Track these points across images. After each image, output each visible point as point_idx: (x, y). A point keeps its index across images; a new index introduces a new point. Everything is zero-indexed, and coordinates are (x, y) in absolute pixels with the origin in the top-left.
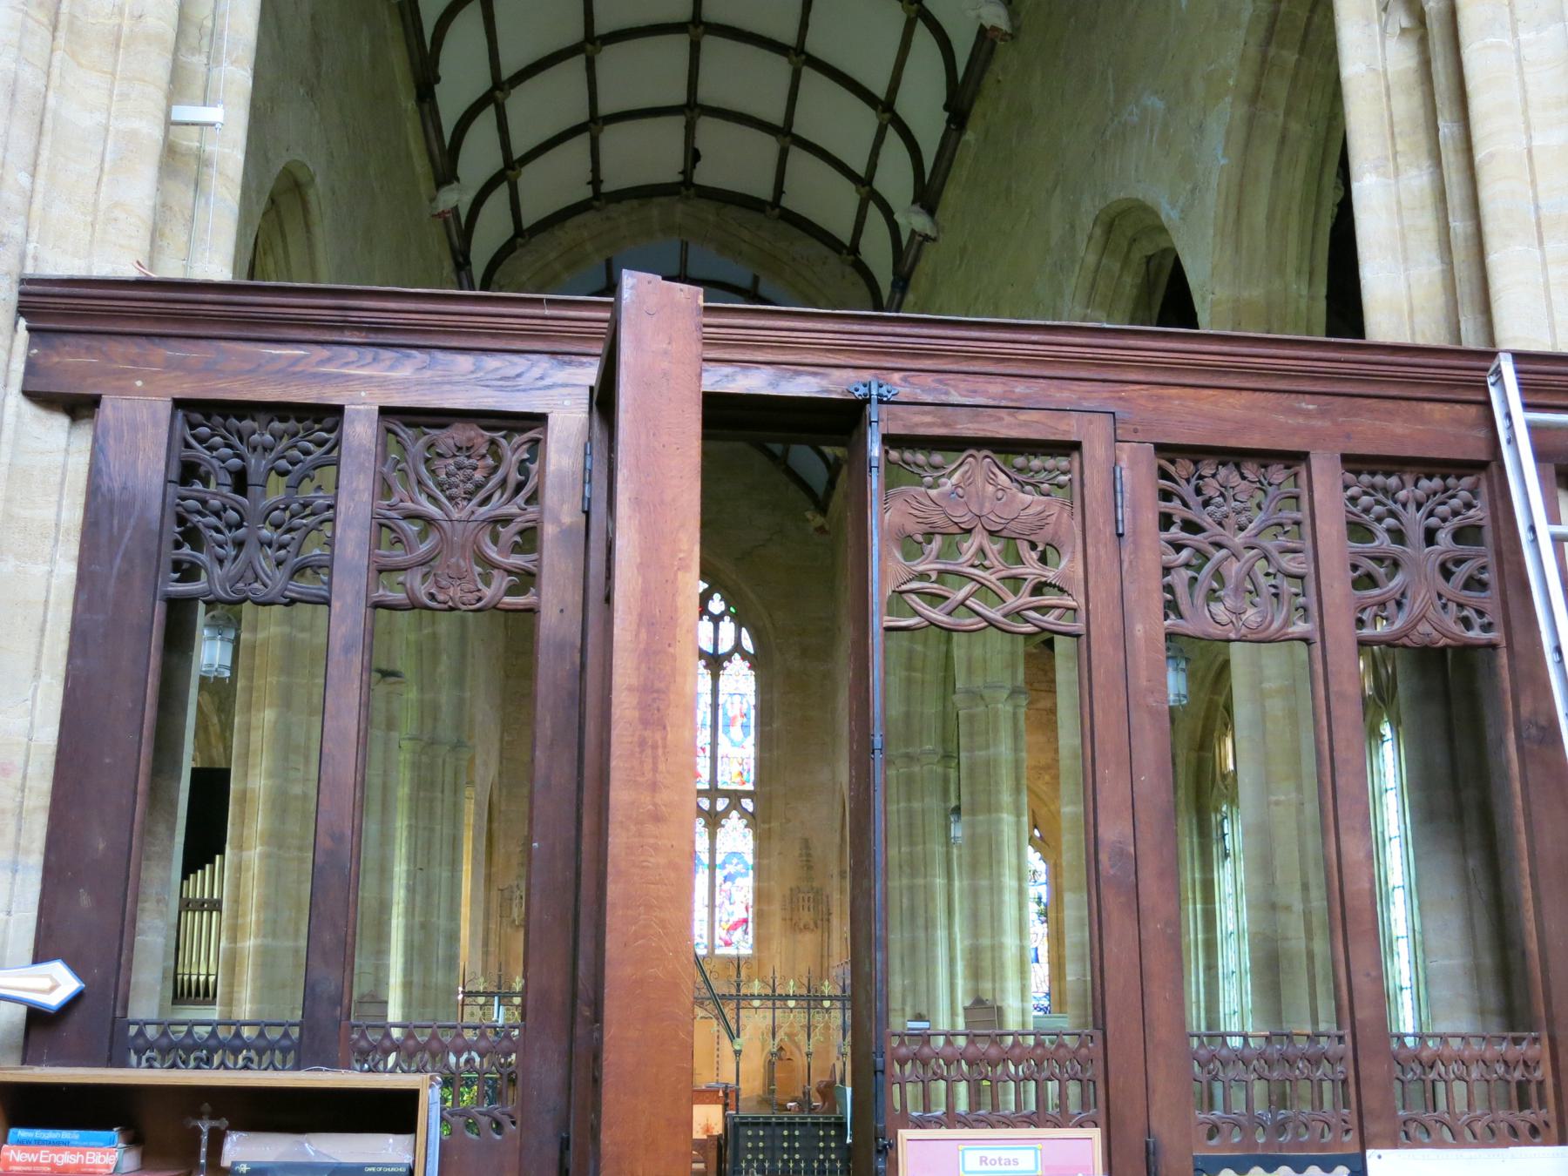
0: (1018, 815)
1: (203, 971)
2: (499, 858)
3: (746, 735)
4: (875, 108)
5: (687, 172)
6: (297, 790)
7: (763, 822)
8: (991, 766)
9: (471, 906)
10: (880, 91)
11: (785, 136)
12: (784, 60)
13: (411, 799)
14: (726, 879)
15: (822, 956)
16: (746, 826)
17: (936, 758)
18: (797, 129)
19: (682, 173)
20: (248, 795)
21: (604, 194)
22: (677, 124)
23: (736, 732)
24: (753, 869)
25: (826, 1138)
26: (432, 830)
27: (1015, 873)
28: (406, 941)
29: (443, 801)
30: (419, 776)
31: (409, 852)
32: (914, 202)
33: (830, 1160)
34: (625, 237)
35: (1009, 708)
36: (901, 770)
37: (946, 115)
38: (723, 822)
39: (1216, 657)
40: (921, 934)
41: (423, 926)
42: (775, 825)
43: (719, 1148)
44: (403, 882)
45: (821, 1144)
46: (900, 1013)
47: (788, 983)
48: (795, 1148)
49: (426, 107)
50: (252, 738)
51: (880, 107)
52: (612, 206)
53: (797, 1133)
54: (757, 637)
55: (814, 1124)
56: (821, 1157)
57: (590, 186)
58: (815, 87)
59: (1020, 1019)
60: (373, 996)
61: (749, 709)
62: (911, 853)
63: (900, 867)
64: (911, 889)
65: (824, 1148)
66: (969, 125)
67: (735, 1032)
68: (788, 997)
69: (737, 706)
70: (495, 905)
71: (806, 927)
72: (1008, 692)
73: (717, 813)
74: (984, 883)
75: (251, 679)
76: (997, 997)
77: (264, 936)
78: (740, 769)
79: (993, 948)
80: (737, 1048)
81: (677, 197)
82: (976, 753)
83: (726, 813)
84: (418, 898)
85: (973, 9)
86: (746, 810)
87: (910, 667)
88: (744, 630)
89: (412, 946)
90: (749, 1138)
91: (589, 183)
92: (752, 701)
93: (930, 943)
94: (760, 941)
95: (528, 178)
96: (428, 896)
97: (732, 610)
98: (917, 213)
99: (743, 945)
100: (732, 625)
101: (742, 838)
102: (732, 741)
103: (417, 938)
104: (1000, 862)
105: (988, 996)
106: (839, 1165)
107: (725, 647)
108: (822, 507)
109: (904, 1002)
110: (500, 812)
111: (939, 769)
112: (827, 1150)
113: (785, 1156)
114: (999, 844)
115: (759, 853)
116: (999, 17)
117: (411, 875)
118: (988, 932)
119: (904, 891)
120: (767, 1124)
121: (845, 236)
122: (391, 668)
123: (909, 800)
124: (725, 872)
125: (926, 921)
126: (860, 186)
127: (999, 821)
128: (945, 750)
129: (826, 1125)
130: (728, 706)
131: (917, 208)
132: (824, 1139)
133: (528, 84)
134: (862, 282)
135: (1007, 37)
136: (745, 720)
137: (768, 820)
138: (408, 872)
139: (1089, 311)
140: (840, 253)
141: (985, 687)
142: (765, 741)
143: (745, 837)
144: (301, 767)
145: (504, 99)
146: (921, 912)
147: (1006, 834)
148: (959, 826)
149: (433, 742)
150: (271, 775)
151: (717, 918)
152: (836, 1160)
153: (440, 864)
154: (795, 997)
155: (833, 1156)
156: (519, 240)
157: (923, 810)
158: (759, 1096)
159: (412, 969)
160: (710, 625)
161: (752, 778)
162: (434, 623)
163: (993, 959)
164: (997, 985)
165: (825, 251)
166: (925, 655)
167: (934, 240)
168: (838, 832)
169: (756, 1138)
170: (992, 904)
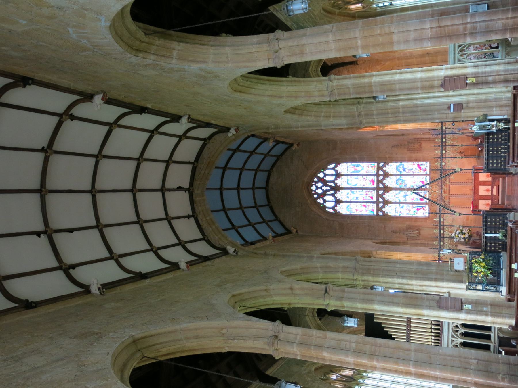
0: (373, 76)
1: (430, 337)
4: (153, 136)
5: (185, 190)
6: (354, 345)
7: (387, 159)
8: (355, 87)
10: (148, 135)
11: (169, 162)
12: (142, 164)
14: (405, 171)
15: (430, 140)
16: (388, 165)
17: (359, 106)
19: (185, 191)
20: (356, 363)
21: (193, 214)
22: (167, 194)
23: (359, 169)
24: (401, 163)
25: (493, 139)
26: (384, 270)
27: (394, 76)
30: (366, 273)
31: (390, 278)
32: (179, 123)
33: (501, 137)
34: (205, 208)
35: (336, 81)
36: (363, 118)
37: (143, 114)
38: (387, 172)
39: (322, 14)
40: (419, 109)
44: (400, 280)
45: (496, 140)
46: (448, 115)
48: (497, 149)
49: (148, 276)
51: (152, 134)
52: (196, 211)
58: (150, 153)
59: (449, 70)
60: (438, 302)
61: (352, 165)
62: (392, 114)
63: (396, 117)
65: (497, 139)
66: (144, 106)
67: (454, 171)
68: (441, 153)
69: (351, 168)
70: (413, 242)
71: (420, 146)
72: (329, 82)
73: (384, 174)
74: (397, 86)
75: (314, 358)
76: (440, 79)
77: (409, 364)
78: (370, 167)
79: (422, 82)
80: (459, 170)
81: (193, 192)
83: (384, 171)
84: (406, 275)
85: (97, 106)
86: (383, 165)
87: (329, 117)
88: (328, 167)
89: (422, 278)
90: (493, 165)
91: (189, 219)
92: (349, 164)
93: (423, 105)
94: (425, 160)
96: (405, 272)
97: (322, 170)
98: (182, 121)
99: (426, 165)
100: (327, 170)
101: (392, 166)
102: (362, 170)
103: (420, 276)
104: (390, 81)
105: (440, 82)
106: (503, 134)
108: (291, 145)
109: (443, 113)
110: (384, 239)
111: (363, 105)
113: (500, 153)
114: (383, 82)
115: (396, 161)
116: (99, 98)
120: (488, 159)
121: (201, 143)
122: (324, 290)
123: (373, 115)
124: (403, 171)
125: (415, 107)
126: (182, 139)
127: (375, 82)
128: (357, 104)
129: (488, 139)
130: (351, 171)
131: (180, 121)
134: (214, 137)
135: (105, 94)
136: (355, 166)
137: (386, 159)
138: (397, 278)
139: (174, 57)
140: (206, 144)
141: (328, 90)
142: (362, 160)
143: (391, 165)
144: (345, 343)
145: (156, 247)
146: (411, 109)
147: (379, 80)
148: (380, 97)
149: (355, 268)
150: (347, 356)
151: (417, 173)
152: (501, 135)
155: (500, 136)
158: (476, 159)
159: (430, 278)
160: (327, 177)
161: (373, 163)
163: (425, 81)
165: (206, 148)
166: (325, 112)
167: (189, 115)
168: (389, 136)
169: (493, 163)
170: (405, 83)
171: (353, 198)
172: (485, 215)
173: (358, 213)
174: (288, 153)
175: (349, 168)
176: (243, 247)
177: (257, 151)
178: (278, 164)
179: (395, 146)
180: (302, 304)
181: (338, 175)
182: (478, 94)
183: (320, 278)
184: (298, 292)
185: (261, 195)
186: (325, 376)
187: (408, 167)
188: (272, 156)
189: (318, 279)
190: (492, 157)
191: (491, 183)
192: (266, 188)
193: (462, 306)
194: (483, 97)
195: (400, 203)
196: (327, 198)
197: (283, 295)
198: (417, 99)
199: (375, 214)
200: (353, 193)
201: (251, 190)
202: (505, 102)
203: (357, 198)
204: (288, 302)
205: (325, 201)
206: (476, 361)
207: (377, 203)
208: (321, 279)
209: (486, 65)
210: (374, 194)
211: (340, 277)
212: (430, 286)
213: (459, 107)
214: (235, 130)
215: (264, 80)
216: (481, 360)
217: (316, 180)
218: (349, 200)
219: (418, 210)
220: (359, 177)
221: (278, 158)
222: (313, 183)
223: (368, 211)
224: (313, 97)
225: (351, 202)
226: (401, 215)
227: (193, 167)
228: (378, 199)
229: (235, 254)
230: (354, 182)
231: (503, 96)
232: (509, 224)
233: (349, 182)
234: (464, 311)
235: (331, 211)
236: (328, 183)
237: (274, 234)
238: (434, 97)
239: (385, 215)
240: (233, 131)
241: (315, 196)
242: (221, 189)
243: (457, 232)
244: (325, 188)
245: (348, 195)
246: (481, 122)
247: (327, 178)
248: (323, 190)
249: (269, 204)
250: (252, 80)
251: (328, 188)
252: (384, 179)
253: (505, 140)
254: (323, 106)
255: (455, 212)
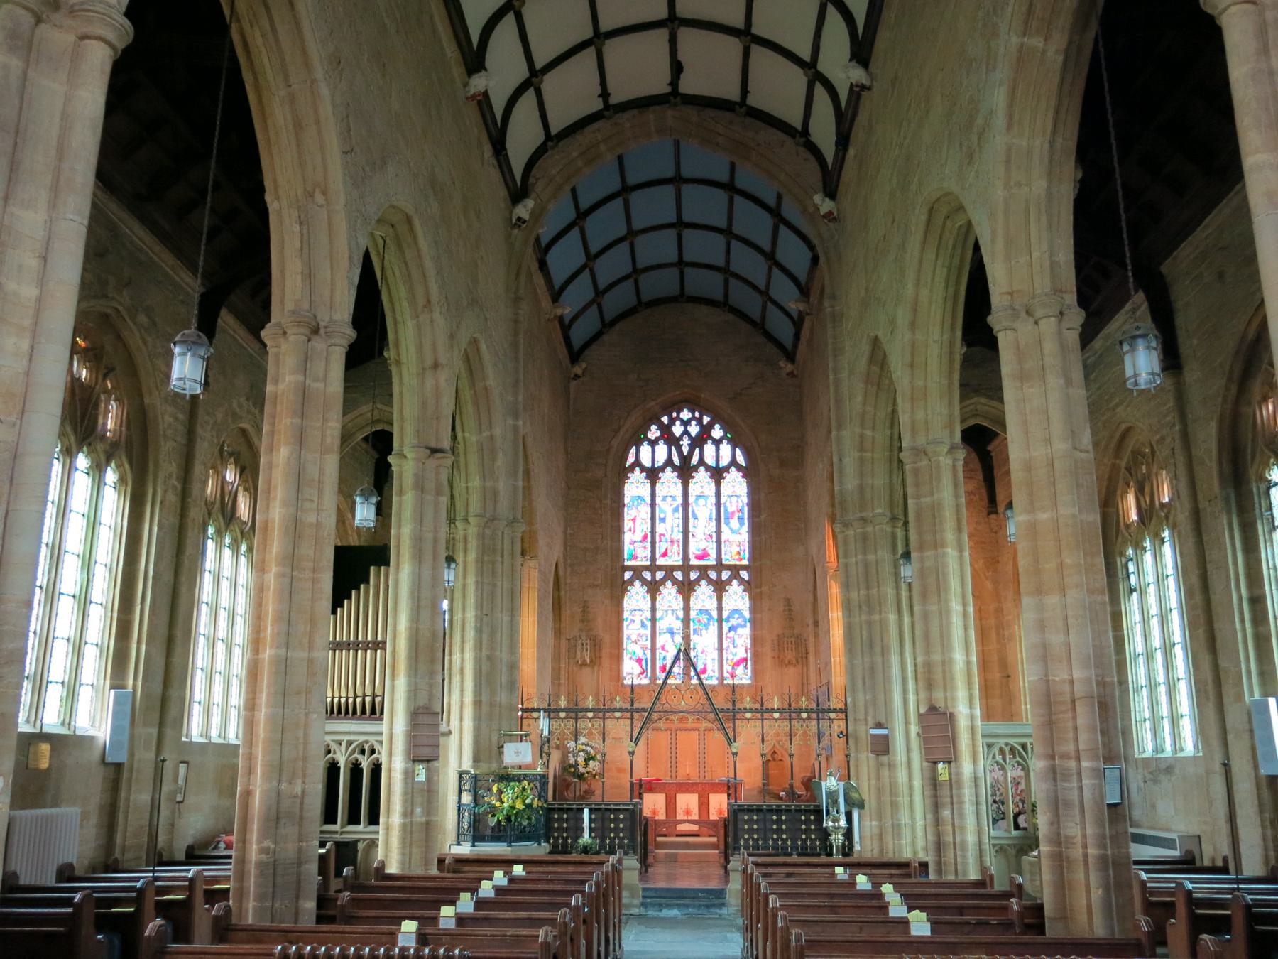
0: (961, 550)
2: (566, 613)
3: (742, 524)
5: (674, 83)
7: (756, 587)
8: (935, 509)
9: (538, 647)
13: (477, 562)
14: (730, 629)
15: (803, 684)
16: (744, 591)
18: (754, 31)
19: (670, 84)
23: (734, 523)
25: (807, 822)
26: (495, 585)
28: (475, 669)
29: (502, 563)
31: (476, 601)
32: (851, 60)
35: (949, 462)
40: (879, 659)
41: (489, 658)
42: (765, 589)
43: (726, 827)
44: (473, 624)
47: (773, 699)
50: (273, 475)
53: (783, 818)
54: (748, 454)
55: (796, 810)
56: (804, 836)
57: (601, 99)
62: (868, 596)
63: (860, 607)
64: (870, 624)
68: (773, 710)
70: (564, 650)
71: (790, 663)
74: (934, 608)
75: (273, 425)
77: (277, 647)
78: (738, 549)
79: (944, 662)
80: (734, 750)
82: (922, 500)
83: (729, 582)
88: (738, 450)
89: (481, 672)
90: (746, 822)
92: (745, 500)
93: (886, 667)
94: (756, 673)
95: (549, 83)
99: (744, 677)
102: (731, 529)
103: (485, 669)
104: (947, 590)
105: (940, 704)
107: (724, 462)
109: (866, 713)
111: (889, 529)
112: (807, 831)
113: (775, 836)
115: (753, 610)
117: (479, 620)
118: (939, 648)
119: (864, 626)
120: (759, 811)
121: (797, 123)
122: (439, 446)
123: (865, 553)
124: (730, 624)
125: (882, 648)
127: (945, 555)
129: (806, 812)
130: (728, 504)
131: (854, 63)
132: (806, 831)
133: (603, 257)
134: (810, 156)
140: (793, 137)
142: (756, 530)
144: (315, 499)
148: (909, 567)
149: (493, 519)
150: (285, 504)
153: (502, 612)
154: (778, 710)
155: (813, 836)
156: (550, 144)
157: (877, 561)
161: (747, 555)
162: (491, 428)
163: (944, 672)
164: (948, 694)
166: (873, 438)
167: (869, 89)
169: (751, 821)
170: (941, 626)
171: (662, 511)
172: (631, 807)
173: (627, 524)
174: (771, 349)
175: (734, 499)
176: (532, 240)
177: (776, 270)
178: (744, 326)
179: (790, 605)
180: (401, 393)
181: (718, 474)
182: (911, 788)
183: (467, 435)
184: (429, 382)
185: (660, 284)
186: (231, 454)
187: (740, 636)
188: (764, 308)
189: (463, 431)
190: (765, 820)
191: (704, 818)
192: (683, 297)
193: (422, 761)
194: (903, 800)
195: (654, 620)
196: (662, 450)
197: (420, 347)
198: (902, 654)
199: (626, 563)
200: (676, 510)
201: (675, 259)
202: (890, 846)
203: (663, 520)
204: (404, 360)
205: (653, 443)
206: (299, 794)
207: (653, 568)
208: (464, 438)
209: (977, 803)
210: (675, 559)
211: (469, 485)
212: (462, 691)
213: (882, 747)
214: (830, 213)
215: (958, 283)
216: (302, 803)
217: (706, 420)
218: (658, 500)
219: (639, 661)
220: (714, 523)
221: (759, 326)
222: (697, 414)
223: (632, 547)
224: (912, 408)
225: (653, 505)
226: (625, 624)
227: (736, 103)
228: (661, 568)
229: (514, 220)
230: (703, 511)
231: (906, 840)
232: (613, 859)
233: (701, 502)
234: (410, 765)
235: (631, 460)
236: (697, 450)
237: (567, 321)
238: (905, 691)
239: (623, 587)
240: (826, 206)
241: (665, 420)
242: (677, 180)
243: (589, 749)
244: (685, 443)
245: (669, 499)
246: (845, 794)
247: (709, 448)
248: (681, 438)
249: (642, 306)
250: (959, 251)
251: (685, 450)
252: (710, 581)
253: (804, 847)
254: (888, 432)
255: (636, 743)
